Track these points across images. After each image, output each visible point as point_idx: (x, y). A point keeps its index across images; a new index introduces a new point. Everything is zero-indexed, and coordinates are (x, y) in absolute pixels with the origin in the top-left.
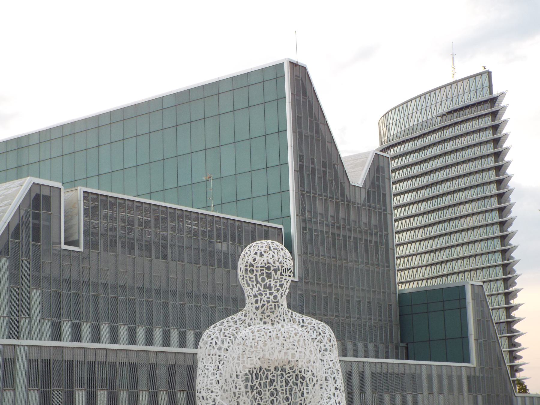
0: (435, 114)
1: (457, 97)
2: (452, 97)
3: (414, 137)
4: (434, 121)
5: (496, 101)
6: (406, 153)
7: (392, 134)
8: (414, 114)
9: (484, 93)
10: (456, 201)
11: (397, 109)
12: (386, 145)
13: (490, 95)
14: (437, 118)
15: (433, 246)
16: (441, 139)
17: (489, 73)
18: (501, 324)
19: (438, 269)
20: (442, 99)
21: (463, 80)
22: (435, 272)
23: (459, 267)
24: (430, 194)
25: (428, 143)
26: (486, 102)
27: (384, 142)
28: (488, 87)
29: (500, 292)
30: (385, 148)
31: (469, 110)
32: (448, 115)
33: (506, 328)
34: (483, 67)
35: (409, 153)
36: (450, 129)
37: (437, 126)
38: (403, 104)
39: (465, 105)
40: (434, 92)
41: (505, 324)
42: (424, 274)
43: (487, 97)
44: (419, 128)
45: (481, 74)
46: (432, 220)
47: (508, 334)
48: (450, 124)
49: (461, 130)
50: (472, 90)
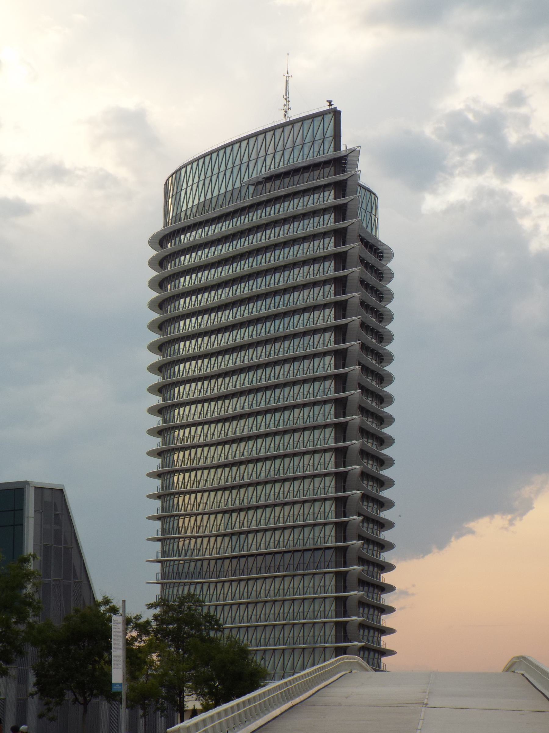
0: (246, 179)
1: (301, 146)
3: (241, 207)
5: (345, 163)
6: (197, 245)
7: (184, 208)
9: (325, 148)
12: (173, 226)
14: (248, 188)
15: (262, 403)
17: (336, 114)
19: (268, 444)
20: (285, 145)
21: (302, 120)
26: (326, 163)
28: (331, 138)
31: (319, 171)
33: (333, 558)
34: (328, 101)
35: (202, 246)
37: (248, 202)
39: (312, 163)
40: (263, 135)
43: (331, 154)
44: (220, 202)
45: (322, 114)
46: (263, 358)
47: (336, 568)
48: (326, 183)
49: (303, 206)
50: (306, 141)
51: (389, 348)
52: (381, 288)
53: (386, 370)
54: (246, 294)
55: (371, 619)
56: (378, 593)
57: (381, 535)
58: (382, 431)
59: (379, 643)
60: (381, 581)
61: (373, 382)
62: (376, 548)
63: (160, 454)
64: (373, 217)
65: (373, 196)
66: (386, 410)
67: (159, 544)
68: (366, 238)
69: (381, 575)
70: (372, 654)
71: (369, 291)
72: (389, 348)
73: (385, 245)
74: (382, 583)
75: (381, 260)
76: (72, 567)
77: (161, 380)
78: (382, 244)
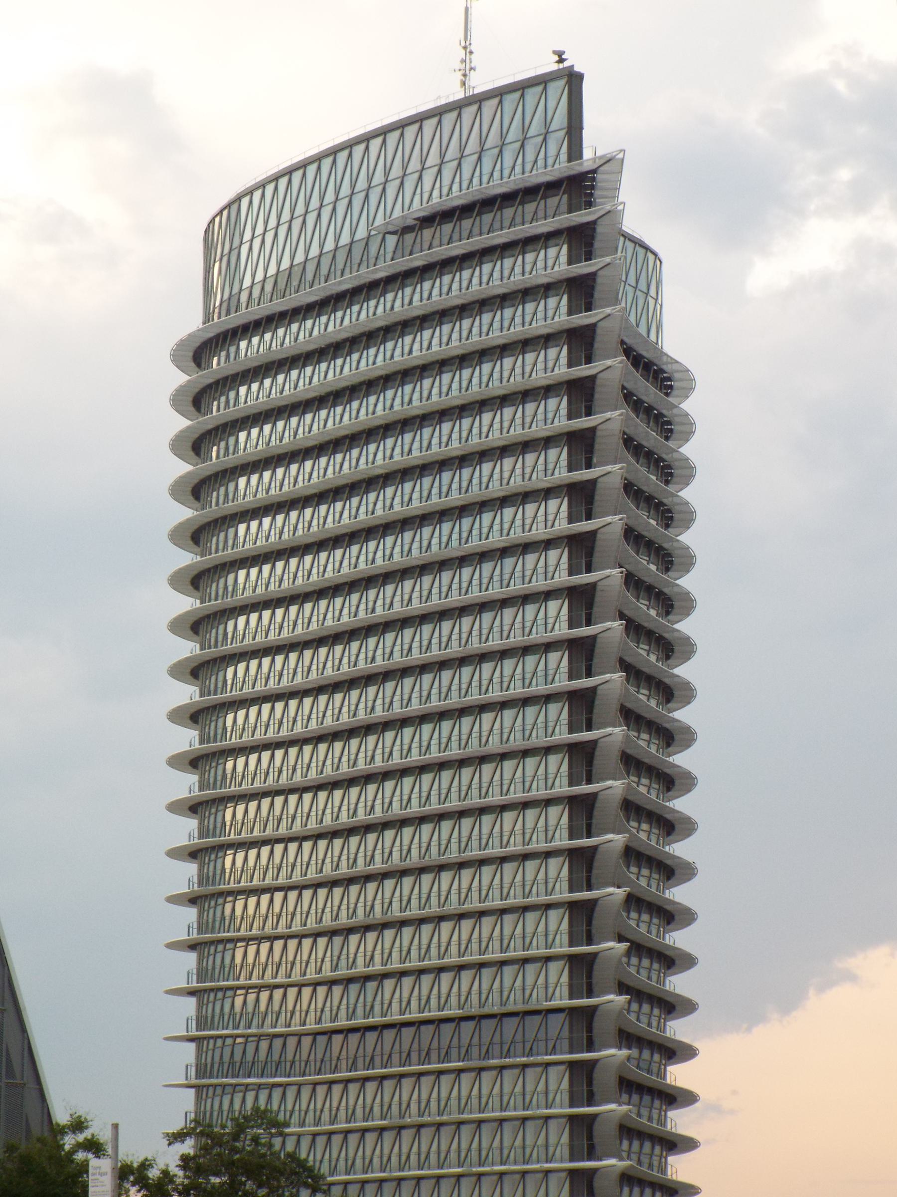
0: (379, 221)
4: (373, 250)
5: (592, 187)
7: (247, 283)
10: (534, 531)
12: (223, 322)
13: (570, 160)
14: (383, 239)
20: (482, 143)
21: (500, 93)
23: (505, 788)
24: (416, 503)
25: (421, 307)
26: (551, 187)
28: (563, 133)
30: (228, 331)
31: (492, 214)
33: (566, 1033)
34: (555, 52)
38: (276, 178)
41: (562, 1016)
44: (324, 270)
45: (542, 81)
47: (571, 1052)
51: (686, 538)
52: (667, 454)
53: (678, 631)
55: (646, 1165)
56: (661, 1108)
57: (667, 982)
58: (671, 759)
59: (663, 1169)
60: (668, 988)
61: (651, 655)
62: (656, 1012)
63: (194, 808)
66: (678, 715)
67: (192, 1001)
69: (669, 1068)
71: (642, 460)
72: (686, 538)
75: (667, 395)
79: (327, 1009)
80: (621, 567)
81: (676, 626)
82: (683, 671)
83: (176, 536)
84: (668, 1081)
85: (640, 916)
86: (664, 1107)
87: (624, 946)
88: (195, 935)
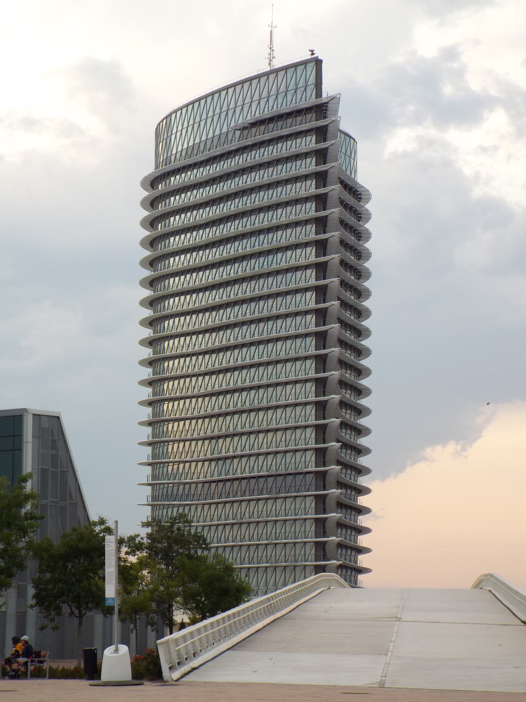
0: (233, 124)
2: (286, 90)
5: (326, 110)
7: (174, 152)
8: (223, 116)
11: (190, 107)
13: (316, 98)
14: (234, 133)
16: (272, 159)
17: (318, 63)
18: (307, 475)
19: (252, 374)
20: (269, 92)
21: (286, 68)
22: (248, 380)
26: (308, 110)
27: (161, 164)
28: (314, 85)
29: (309, 423)
32: (251, 128)
34: (310, 50)
36: (289, 143)
38: (187, 106)
41: (312, 475)
42: (237, 381)
43: (312, 101)
44: (208, 146)
45: (304, 63)
47: (316, 491)
48: (308, 128)
52: (359, 227)
53: (364, 285)
54: (232, 233)
58: (360, 362)
60: (358, 504)
62: (353, 473)
63: (151, 363)
64: (352, 160)
65: (352, 141)
67: (150, 468)
68: (345, 180)
69: (359, 517)
70: (349, 571)
71: (348, 230)
73: (363, 187)
74: (360, 546)
76: (68, 489)
77: (152, 314)
78: (360, 186)
79: (209, 472)
80: (338, 277)
81: (363, 303)
82: (366, 323)
83: (143, 263)
84: (358, 504)
85: (346, 451)
86: (356, 515)
87: (339, 444)
88: (151, 439)
